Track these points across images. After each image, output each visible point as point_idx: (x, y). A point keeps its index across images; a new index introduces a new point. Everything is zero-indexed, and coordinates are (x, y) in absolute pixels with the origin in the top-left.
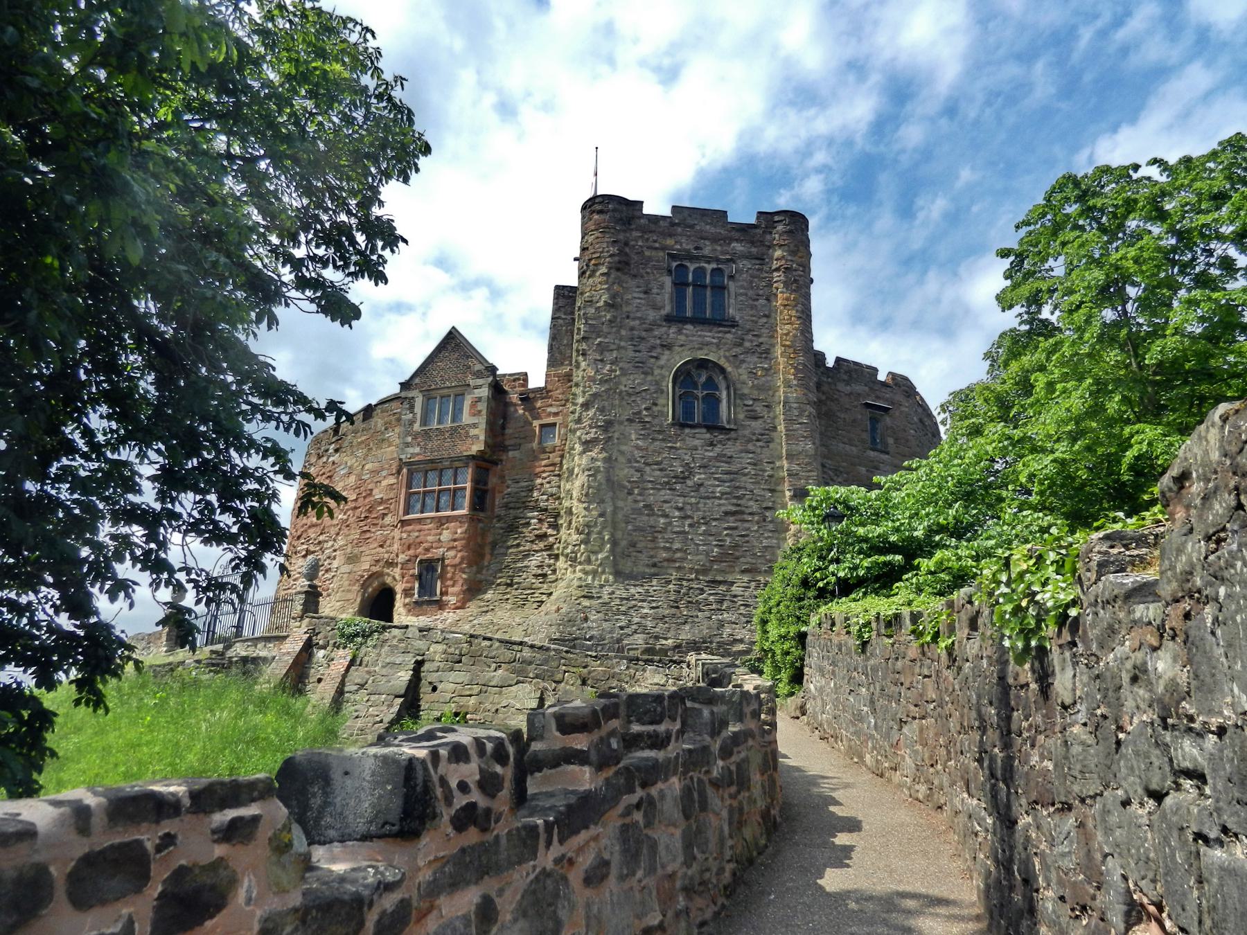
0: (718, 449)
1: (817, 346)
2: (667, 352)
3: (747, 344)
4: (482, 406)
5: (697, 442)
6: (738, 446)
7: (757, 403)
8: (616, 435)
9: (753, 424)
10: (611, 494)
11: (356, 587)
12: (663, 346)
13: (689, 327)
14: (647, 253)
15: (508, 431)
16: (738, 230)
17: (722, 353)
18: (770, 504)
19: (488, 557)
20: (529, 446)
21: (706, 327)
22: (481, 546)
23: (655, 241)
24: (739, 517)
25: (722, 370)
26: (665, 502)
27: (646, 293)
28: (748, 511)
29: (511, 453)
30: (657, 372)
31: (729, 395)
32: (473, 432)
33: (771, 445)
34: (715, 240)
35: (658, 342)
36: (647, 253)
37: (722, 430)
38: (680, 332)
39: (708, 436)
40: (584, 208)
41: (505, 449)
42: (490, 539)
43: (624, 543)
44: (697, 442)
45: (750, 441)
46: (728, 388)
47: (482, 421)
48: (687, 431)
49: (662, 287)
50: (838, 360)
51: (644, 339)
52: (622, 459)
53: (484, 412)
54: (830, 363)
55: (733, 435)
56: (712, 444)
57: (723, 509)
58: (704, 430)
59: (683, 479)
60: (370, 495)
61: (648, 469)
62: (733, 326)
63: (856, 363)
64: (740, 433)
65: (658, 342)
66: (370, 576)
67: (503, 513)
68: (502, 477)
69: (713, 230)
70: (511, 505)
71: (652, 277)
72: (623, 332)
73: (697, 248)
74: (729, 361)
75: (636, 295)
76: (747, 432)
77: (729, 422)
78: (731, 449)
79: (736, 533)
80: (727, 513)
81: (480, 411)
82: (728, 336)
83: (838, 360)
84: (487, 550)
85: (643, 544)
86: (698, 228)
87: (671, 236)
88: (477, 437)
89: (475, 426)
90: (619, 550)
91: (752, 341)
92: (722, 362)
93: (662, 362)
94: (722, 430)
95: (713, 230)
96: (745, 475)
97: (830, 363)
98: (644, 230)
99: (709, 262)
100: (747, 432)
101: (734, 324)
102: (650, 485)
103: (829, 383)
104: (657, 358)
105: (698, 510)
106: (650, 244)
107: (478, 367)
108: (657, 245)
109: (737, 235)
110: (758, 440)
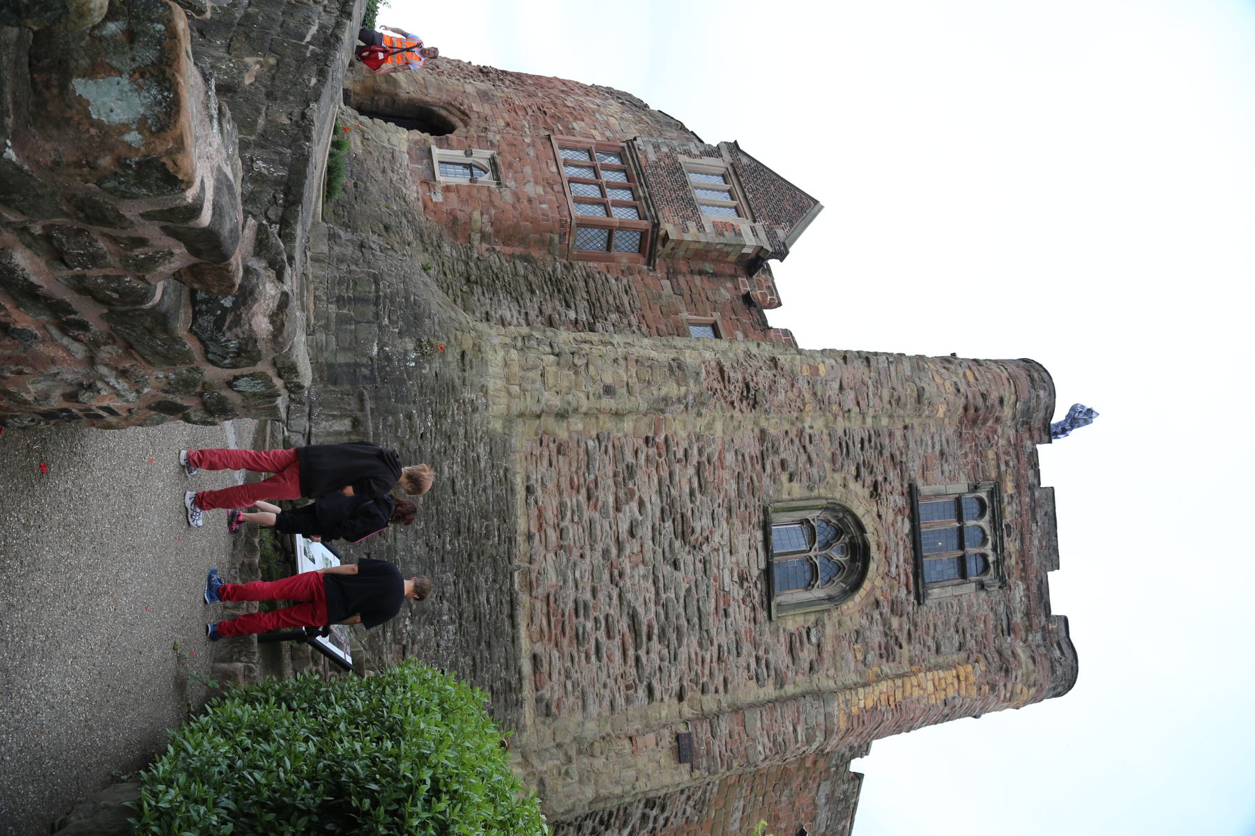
0: (737, 592)
1: (876, 745)
2: (867, 492)
3: (895, 622)
4: (729, 237)
5: (743, 551)
6: (743, 625)
7: (814, 649)
8: (737, 414)
9: (783, 649)
10: (644, 407)
11: (444, 97)
12: (875, 485)
13: (907, 527)
14: (991, 454)
15: (697, 279)
16: (1039, 588)
17: (879, 582)
18: (657, 694)
19: (508, 250)
20: (682, 307)
21: (910, 554)
22: (523, 241)
23: (1007, 464)
24: (630, 641)
25: (856, 587)
26: (641, 504)
27: (942, 453)
28: (642, 653)
29: (667, 283)
30: (838, 477)
31: (820, 601)
32: (692, 225)
33: (753, 683)
34: (1023, 554)
35: (880, 478)
36: (991, 454)
37: (769, 594)
38: (900, 511)
39: (755, 572)
40: (1025, 360)
41: (672, 274)
42: (536, 254)
43: (563, 435)
44: (743, 551)
45: (756, 646)
46: (830, 599)
47: (709, 236)
48: (759, 535)
49: (953, 479)
50: (859, 777)
51: (881, 453)
52: (701, 423)
53: (722, 240)
54: (856, 765)
55: (762, 615)
56: (743, 579)
57: (641, 610)
58: (763, 565)
59: (684, 533)
60: (576, 119)
61: (691, 471)
62: (917, 597)
63: (856, 804)
64: (767, 628)
65: (880, 478)
66: (464, 113)
67: (577, 272)
68: (629, 271)
69: (1034, 552)
70: (591, 283)
71: (962, 461)
72: (885, 421)
73: (1008, 526)
74: (868, 594)
75: (937, 438)
76: (767, 638)
77: (779, 605)
78: (740, 615)
79: (601, 634)
80: (633, 617)
81: (722, 234)
82: (904, 592)
83: (859, 777)
84: (518, 250)
85: (565, 469)
86: (1034, 528)
87: (1017, 486)
88: (685, 230)
89: (701, 228)
90: (549, 423)
91: (901, 629)
92: (867, 585)
93: (853, 485)
94: (769, 594)
95: (1034, 552)
96: (701, 645)
97: (856, 765)
98: (1017, 446)
99: (994, 549)
100: (767, 638)
101: (920, 598)
102: (665, 474)
103: (827, 770)
104: (858, 476)
105: (635, 566)
106: (1003, 458)
107: (781, 233)
108: (1003, 468)
109: (1034, 589)
110: (758, 659)
